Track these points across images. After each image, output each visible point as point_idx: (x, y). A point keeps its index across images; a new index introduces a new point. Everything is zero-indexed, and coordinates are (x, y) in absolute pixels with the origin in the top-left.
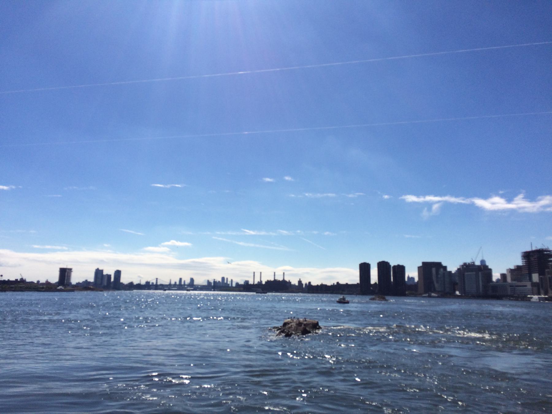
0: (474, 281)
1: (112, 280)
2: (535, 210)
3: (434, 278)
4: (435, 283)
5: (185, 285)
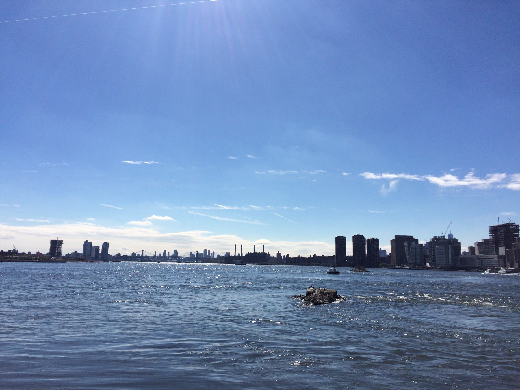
0: (444, 254)
1: (100, 251)
2: (486, 187)
3: (406, 252)
4: (407, 255)
5: (169, 257)
